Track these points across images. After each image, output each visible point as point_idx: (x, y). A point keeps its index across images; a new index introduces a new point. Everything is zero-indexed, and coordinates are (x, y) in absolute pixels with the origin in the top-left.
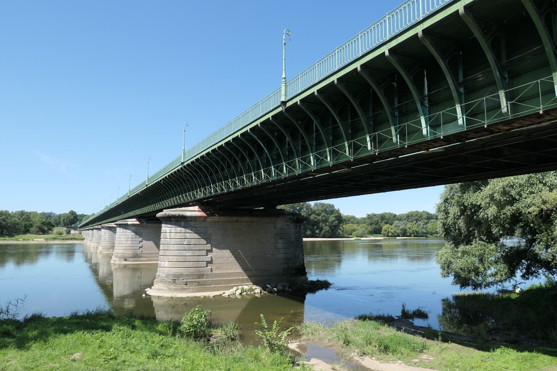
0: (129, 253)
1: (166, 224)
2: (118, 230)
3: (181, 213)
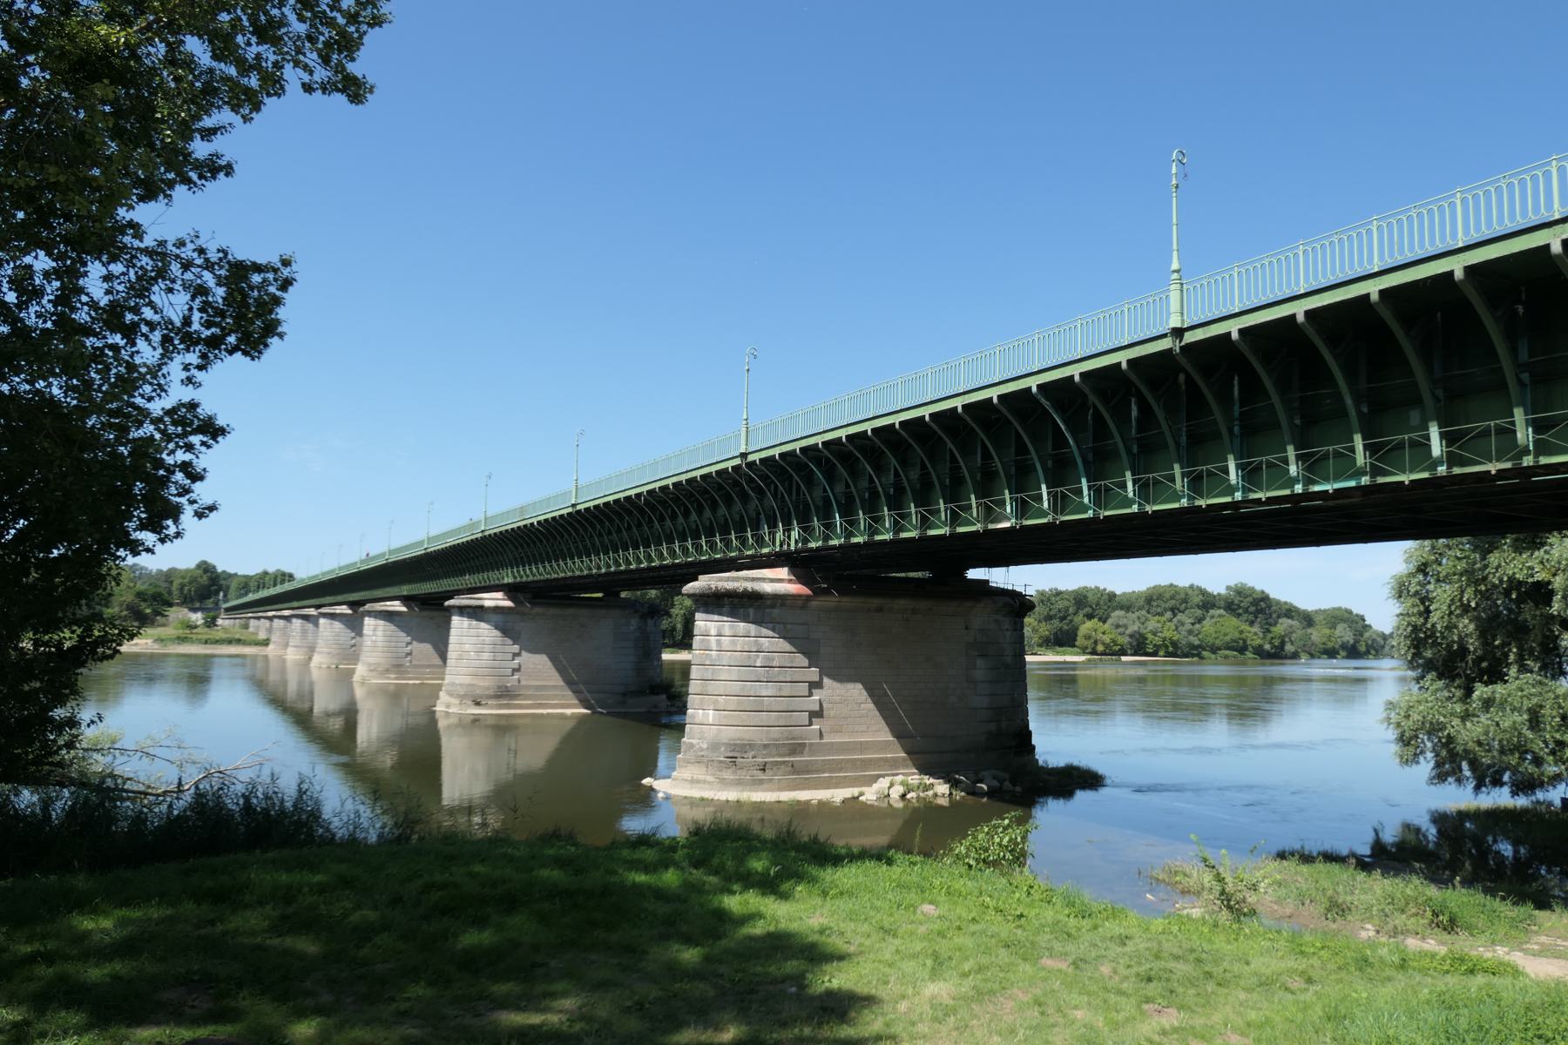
0: (486, 684)
1: (707, 612)
2: (322, 621)
3: (749, 586)
